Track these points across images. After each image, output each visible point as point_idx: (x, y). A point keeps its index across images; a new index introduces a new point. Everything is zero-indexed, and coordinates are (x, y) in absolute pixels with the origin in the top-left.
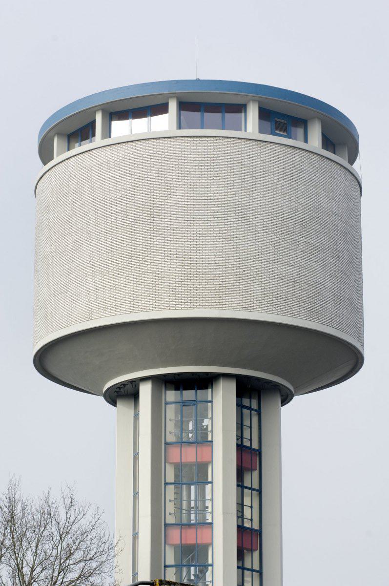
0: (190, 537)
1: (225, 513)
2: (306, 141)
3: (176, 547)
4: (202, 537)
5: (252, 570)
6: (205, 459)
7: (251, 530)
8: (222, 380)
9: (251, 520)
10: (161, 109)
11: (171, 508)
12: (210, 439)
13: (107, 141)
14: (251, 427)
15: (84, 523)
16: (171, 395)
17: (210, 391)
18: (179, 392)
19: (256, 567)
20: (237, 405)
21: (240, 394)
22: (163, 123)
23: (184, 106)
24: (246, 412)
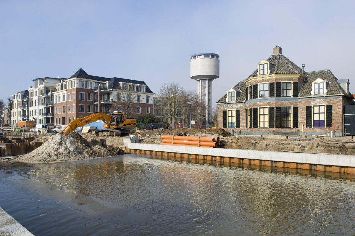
16: (203, 81)
23: (204, 55)
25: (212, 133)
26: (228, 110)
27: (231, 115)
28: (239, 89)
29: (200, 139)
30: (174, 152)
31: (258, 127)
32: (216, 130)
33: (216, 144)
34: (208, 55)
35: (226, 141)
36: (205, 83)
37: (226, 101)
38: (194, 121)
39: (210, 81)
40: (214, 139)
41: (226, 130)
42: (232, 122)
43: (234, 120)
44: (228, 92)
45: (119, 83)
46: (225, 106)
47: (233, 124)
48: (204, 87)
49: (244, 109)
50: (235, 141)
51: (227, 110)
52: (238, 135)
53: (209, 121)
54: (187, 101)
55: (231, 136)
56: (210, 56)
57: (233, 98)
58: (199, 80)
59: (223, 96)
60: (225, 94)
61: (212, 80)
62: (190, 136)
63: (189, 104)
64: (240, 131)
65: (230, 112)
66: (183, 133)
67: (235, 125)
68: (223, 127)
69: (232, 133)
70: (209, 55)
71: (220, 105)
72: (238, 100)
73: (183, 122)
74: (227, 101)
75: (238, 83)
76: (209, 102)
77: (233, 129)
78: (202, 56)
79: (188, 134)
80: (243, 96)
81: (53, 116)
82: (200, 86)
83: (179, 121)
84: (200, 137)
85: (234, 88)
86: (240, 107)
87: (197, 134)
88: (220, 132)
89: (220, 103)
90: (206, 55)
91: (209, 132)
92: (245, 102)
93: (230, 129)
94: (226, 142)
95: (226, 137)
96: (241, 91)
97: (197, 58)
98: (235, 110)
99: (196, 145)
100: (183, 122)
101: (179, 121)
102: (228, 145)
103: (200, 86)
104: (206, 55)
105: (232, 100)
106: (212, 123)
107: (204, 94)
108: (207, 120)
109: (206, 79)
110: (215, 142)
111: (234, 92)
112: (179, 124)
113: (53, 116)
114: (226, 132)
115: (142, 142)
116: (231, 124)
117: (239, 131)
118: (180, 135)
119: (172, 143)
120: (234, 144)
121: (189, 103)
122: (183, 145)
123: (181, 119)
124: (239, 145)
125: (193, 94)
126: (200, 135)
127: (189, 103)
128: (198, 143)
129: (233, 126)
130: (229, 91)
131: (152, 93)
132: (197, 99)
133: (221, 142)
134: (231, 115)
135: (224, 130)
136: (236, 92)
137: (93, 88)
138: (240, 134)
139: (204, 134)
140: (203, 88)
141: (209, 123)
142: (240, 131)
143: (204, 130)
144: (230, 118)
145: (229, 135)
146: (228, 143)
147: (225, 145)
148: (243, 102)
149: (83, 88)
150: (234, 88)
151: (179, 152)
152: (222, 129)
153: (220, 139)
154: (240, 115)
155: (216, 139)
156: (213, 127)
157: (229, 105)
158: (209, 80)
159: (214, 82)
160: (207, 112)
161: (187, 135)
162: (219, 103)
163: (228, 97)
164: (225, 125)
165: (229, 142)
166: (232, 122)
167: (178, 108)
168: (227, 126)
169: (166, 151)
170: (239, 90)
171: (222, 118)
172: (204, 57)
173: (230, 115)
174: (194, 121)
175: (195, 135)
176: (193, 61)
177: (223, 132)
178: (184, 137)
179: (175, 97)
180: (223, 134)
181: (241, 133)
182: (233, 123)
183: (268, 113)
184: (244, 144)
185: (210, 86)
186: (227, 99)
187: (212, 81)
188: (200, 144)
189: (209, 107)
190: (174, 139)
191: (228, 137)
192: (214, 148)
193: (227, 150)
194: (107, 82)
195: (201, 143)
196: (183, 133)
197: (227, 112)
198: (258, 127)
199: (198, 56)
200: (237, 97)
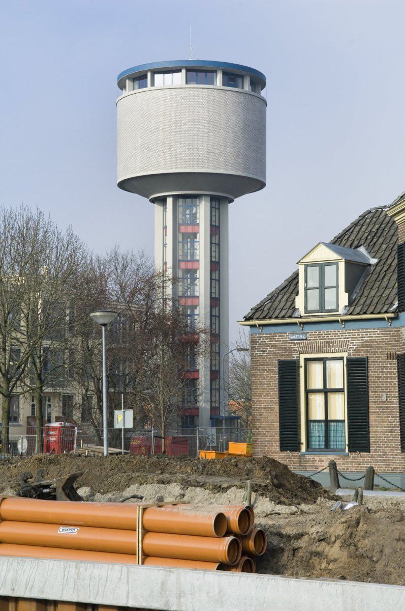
0: (190, 266)
1: (205, 256)
2: (243, 88)
3: (183, 270)
4: (195, 302)
5: (215, 280)
6: (196, 232)
7: (215, 226)
8: (203, 202)
9: (215, 257)
10: (179, 71)
11: (180, 252)
12: (198, 222)
13: (153, 88)
14: (215, 324)
15: (148, 264)
16: (181, 202)
17: (198, 199)
18: (184, 200)
19: (217, 278)
20: (210, 207)
21: (211, 200)
22: (180, 77)
23: (188, 70)
24: (213, 209)
25: (217, 480)
26: (306, 360)
27: (320, 386)
28: (362, 250)
29: (149, 516)
30: (74, 599)
31: (303, 448)
32: (241, 466)
33: (233, 545)
35: (289, 531)
36: (194, 216)
37: (295, 309)
38: (130, 414)
39: (219, 202)
40: (220, 518)
41: (295, 468)
42: (327, 422)
43: (339, 408)
44: (307, 266)
46: (291, 335)
47: (332, 434)
48: (186, 236)
49: (390, 356)
50: (338, 529)
51: (302, 357)
52: (358, 497)
53: (214, 410)
54: (98, 305)
55: (320, 500)
56: (219, 78)
57: (329, 295)
58: (162, 201)
59: (279, 281)
60: (289, 274)
61: (231, 201)
62: (98, 495)
63: (101, 321)
64: (371, 472)
65: (316, 370)
66: (54, 480)
67: (342, 437)
68: (283, 448)
69: (325, 481)
70: (215, 71)
71: (267, 329)
72: (358, 309)
73: (77, 415)
74: (302, 312)
75: (355, 217)
76: (215, 312)
77: (332, 457)
78: (176, 75)
79: (85, 484)
80: (384, 284)
82: (165, 228)
83: (55, 410)
84: (144, 510)
85: (338, 243)
86: (369, 345)
87: (132, 490)
88: (259, 477)
89: (264, 318)
91: (201, 479)
92: (396, 318)
93: (317, 458)
94: (289, 537)
95: (294, 509)
96: (374, 261)
97: (153, 84)
98: (342, 358)
99: (126, 552)
100: (77, 415)
101: (55, 410)
102: (300, 553)
103: (165, 228)
105: (327, 307)
106: (231, 420)
107: (187, 271)
108: (204, 404)
110: (229, 539)
111: (335, 263)
112: (54, 429)
114: (293, 475)
115: (290, 572)
116: (322, 434)
117: (364, 469)
118: (42, 496)
119: (132, 553)
120: (334, 551)
121: (98, 316)
122: (109, 555)
123: (67, 400)
124: (362, 556)
125: (129, 271)
126: (149, 491)
127: (98, 316)
128: (134, 539)
129: (332, 439)
130: (310, 259)
132: (148, 296)
133: (261, 534)
134: (320, 386)
135: (285, 467)
136: (348, 264)
138: (371, 486)
139: (175, 489)
140: (184, 242)
141: (216, 421)
142: (371, 472)
143: (176, 465)
144: (317, 400)
145: (310, 494)
146: (302, 543)
147: (282, 550)
148: (385, 316)
150: (338, 243)
151: (27, 595)
152: (274, 463)
153: (259, 521)
154: (371, 385)
155: (233, 518)
156: (231, 444)
157: (311, 331)
158: (213, 199)
160: (203, 365)
161: (82, 492)
162: (257, 322)
163: (306, 289)
164: (289, 441)
165: (306, 538)
166: (327, 422)
167: (46, 343)
168: (303, 439)
169: (66, 598)
170: (361, 255)
171: (276, 397)
173: (317, 383)
174: (130, 414)
175: (128, 492)
176: (133, 97)
177: (276, 477)
178: (61, 508)
179: (35, 282)
180: (279, 486)
181: (377, 480)
182: (332, 426)
183: (341, 387)
184: (387, 551)
185: (216, 230)
186: (299, 302)
187: (230, 205)
188: (146, 551)
189: (216, 336)
190: (146, 531)
191: (303, 507)
192: (222, 573)
193: (293, 582)
195: (155, 542)
196: (54, 480)
197: (302, 371)
198: (300, 443)
199: (155, 72)
200: (349, 289)
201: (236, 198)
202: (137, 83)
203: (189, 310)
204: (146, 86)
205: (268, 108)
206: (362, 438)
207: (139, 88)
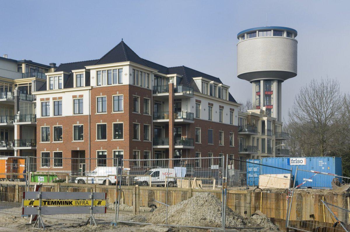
10: (270, 30)
13: (259, 37)
34: (278, 31)
39: (280, 82)
45: (194, 79)
56: (285, 35)
61: (283, 81)
70: (283, 31)
78: (269, 32)
81: (34, 148)
90: (278, 32)
104: (278, 32)
109: (273, 80)
113: (34, 148)
131: (236, 102)
137: (151, 88)
149: (137, 86)
159: (285, 84)
172: (274, 35)
176: (248, 42)
187: (282, 83)
194: (175, 75)
201: (285, 80)
202: (249, 35)
203: (136, 120)
204: (256, 37)
205: (298, 44)
206: (273, 171)
207: (250, 38)
